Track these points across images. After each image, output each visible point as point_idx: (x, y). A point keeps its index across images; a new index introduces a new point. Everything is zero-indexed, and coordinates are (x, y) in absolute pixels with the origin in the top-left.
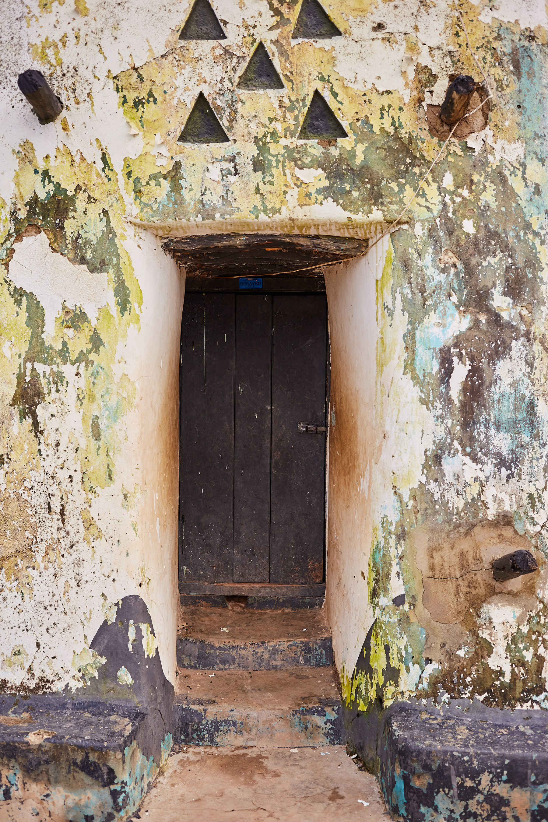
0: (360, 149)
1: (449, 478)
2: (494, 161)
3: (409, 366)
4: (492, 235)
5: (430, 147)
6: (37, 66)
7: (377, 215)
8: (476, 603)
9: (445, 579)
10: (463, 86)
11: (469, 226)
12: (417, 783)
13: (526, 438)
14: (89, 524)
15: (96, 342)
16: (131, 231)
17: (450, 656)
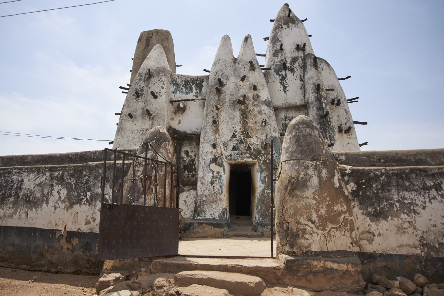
3: (260, 179)
10: (266, 144)
11: (268, 161)
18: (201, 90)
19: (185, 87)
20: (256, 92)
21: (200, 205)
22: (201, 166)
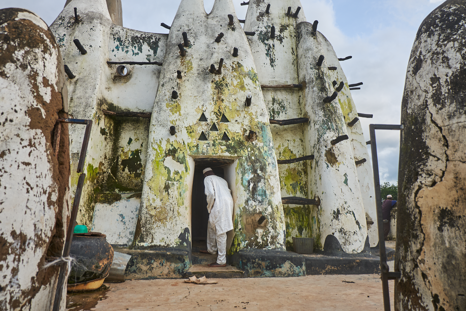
0: (233, 143)
1: (250, 205)
2: (258, 146)
3: (242, 184)
4: (258, 159)
5: (246, 143)
6: (438, 294)
7: (236, 155)
8: (255, 229)
9: (249, 224)
10: (252, 132)
11: (253, 158)
12: (244, 261)
13: (264, 197)
14: (178, 213)
15: (181, 177)
16: (188, 156)
17: (250, 239)
18: (155, 52)
19: (132, 46)
20: (236, 59)
21: (146, 222)
22: (150, 161)
